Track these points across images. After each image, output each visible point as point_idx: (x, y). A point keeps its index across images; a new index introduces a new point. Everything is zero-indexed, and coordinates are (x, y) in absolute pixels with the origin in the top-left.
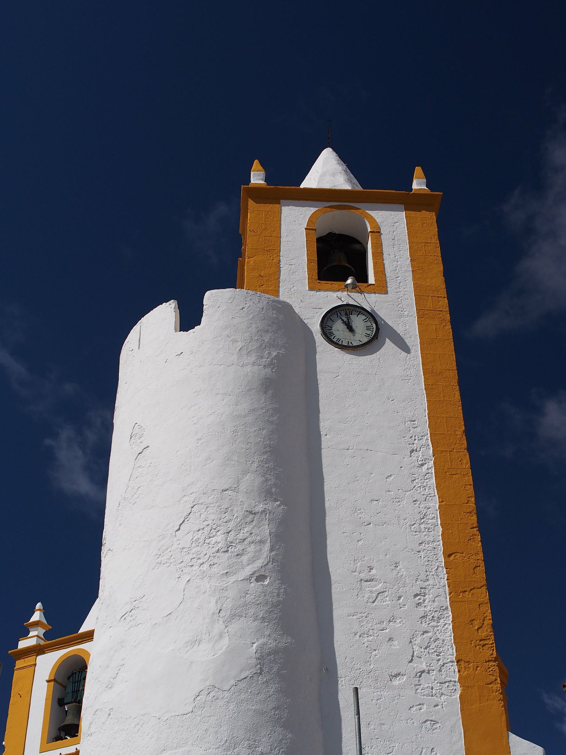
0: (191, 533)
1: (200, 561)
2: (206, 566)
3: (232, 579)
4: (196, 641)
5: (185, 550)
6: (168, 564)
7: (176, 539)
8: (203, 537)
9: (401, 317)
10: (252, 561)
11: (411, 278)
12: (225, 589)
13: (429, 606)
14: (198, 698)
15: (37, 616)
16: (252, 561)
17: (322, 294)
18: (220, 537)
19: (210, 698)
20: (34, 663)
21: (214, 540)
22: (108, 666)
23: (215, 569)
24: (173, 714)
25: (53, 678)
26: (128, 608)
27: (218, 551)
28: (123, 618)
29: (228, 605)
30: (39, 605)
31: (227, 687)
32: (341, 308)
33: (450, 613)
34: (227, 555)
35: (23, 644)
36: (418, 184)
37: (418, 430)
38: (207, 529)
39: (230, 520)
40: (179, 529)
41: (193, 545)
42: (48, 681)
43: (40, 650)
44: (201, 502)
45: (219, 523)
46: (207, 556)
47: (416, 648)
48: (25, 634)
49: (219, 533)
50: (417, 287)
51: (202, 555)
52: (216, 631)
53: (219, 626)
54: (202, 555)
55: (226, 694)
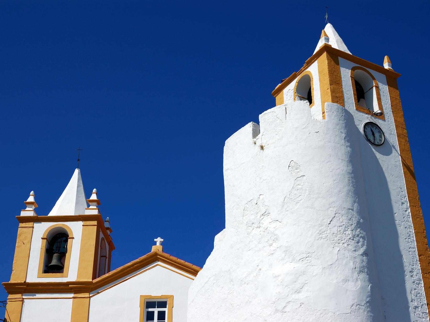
0: (336, 227)
1: (343, 242)
2: (345, 245)
3: (357, 253)
4: (346, 280)
5: (334, 235)
6: (326, 239)
7: (328, 228)
8: (342, 230)
9: (391, 134)
10: (362, 246)
11: (392, 115)
12: (355, 258)
13: (415, 278)
14: (353, 307)
15: (31, 199)
16: (362, 246)
17: (361, 114)
18: (349, 232)
19: (357, 308)
20: (32, 226)
21: (347, 232)
22: (295, 282)
23: (350, 247)
24: (341, 312)
25: (45, 237)
26: (305, 255)
27: (350, 239)
28: (301, 260)
29: (358, 265)
30: (32, 193)
31: (363, 304)
32: (378, 127)
33: (422, 282)
34: (354, 241)
35: (23, 214)
36: (386, 66)
37: (403, 193)
38: (343, 227)
39: (352, 224)
40: (330, 224)
41: (338, 233)
42: (42, 239)
43: (36, 219)
44: (339, 212)
45: (349, 225)
46: (346, 240)
47: (413, 296)
48: (24, 208)
49: (349, 230)
50: (395, 121)
51: (343, 239)
52: (355, 277)
53: (356, 275)
54: (343, 239)
55: (363, 307)
